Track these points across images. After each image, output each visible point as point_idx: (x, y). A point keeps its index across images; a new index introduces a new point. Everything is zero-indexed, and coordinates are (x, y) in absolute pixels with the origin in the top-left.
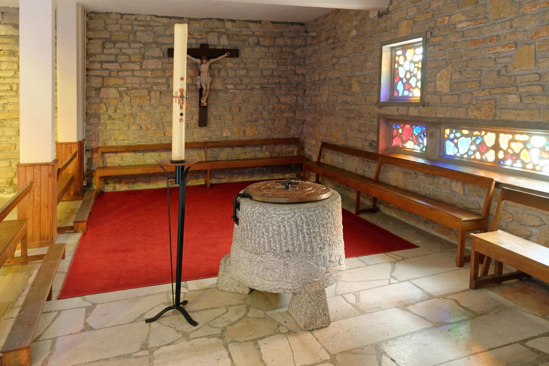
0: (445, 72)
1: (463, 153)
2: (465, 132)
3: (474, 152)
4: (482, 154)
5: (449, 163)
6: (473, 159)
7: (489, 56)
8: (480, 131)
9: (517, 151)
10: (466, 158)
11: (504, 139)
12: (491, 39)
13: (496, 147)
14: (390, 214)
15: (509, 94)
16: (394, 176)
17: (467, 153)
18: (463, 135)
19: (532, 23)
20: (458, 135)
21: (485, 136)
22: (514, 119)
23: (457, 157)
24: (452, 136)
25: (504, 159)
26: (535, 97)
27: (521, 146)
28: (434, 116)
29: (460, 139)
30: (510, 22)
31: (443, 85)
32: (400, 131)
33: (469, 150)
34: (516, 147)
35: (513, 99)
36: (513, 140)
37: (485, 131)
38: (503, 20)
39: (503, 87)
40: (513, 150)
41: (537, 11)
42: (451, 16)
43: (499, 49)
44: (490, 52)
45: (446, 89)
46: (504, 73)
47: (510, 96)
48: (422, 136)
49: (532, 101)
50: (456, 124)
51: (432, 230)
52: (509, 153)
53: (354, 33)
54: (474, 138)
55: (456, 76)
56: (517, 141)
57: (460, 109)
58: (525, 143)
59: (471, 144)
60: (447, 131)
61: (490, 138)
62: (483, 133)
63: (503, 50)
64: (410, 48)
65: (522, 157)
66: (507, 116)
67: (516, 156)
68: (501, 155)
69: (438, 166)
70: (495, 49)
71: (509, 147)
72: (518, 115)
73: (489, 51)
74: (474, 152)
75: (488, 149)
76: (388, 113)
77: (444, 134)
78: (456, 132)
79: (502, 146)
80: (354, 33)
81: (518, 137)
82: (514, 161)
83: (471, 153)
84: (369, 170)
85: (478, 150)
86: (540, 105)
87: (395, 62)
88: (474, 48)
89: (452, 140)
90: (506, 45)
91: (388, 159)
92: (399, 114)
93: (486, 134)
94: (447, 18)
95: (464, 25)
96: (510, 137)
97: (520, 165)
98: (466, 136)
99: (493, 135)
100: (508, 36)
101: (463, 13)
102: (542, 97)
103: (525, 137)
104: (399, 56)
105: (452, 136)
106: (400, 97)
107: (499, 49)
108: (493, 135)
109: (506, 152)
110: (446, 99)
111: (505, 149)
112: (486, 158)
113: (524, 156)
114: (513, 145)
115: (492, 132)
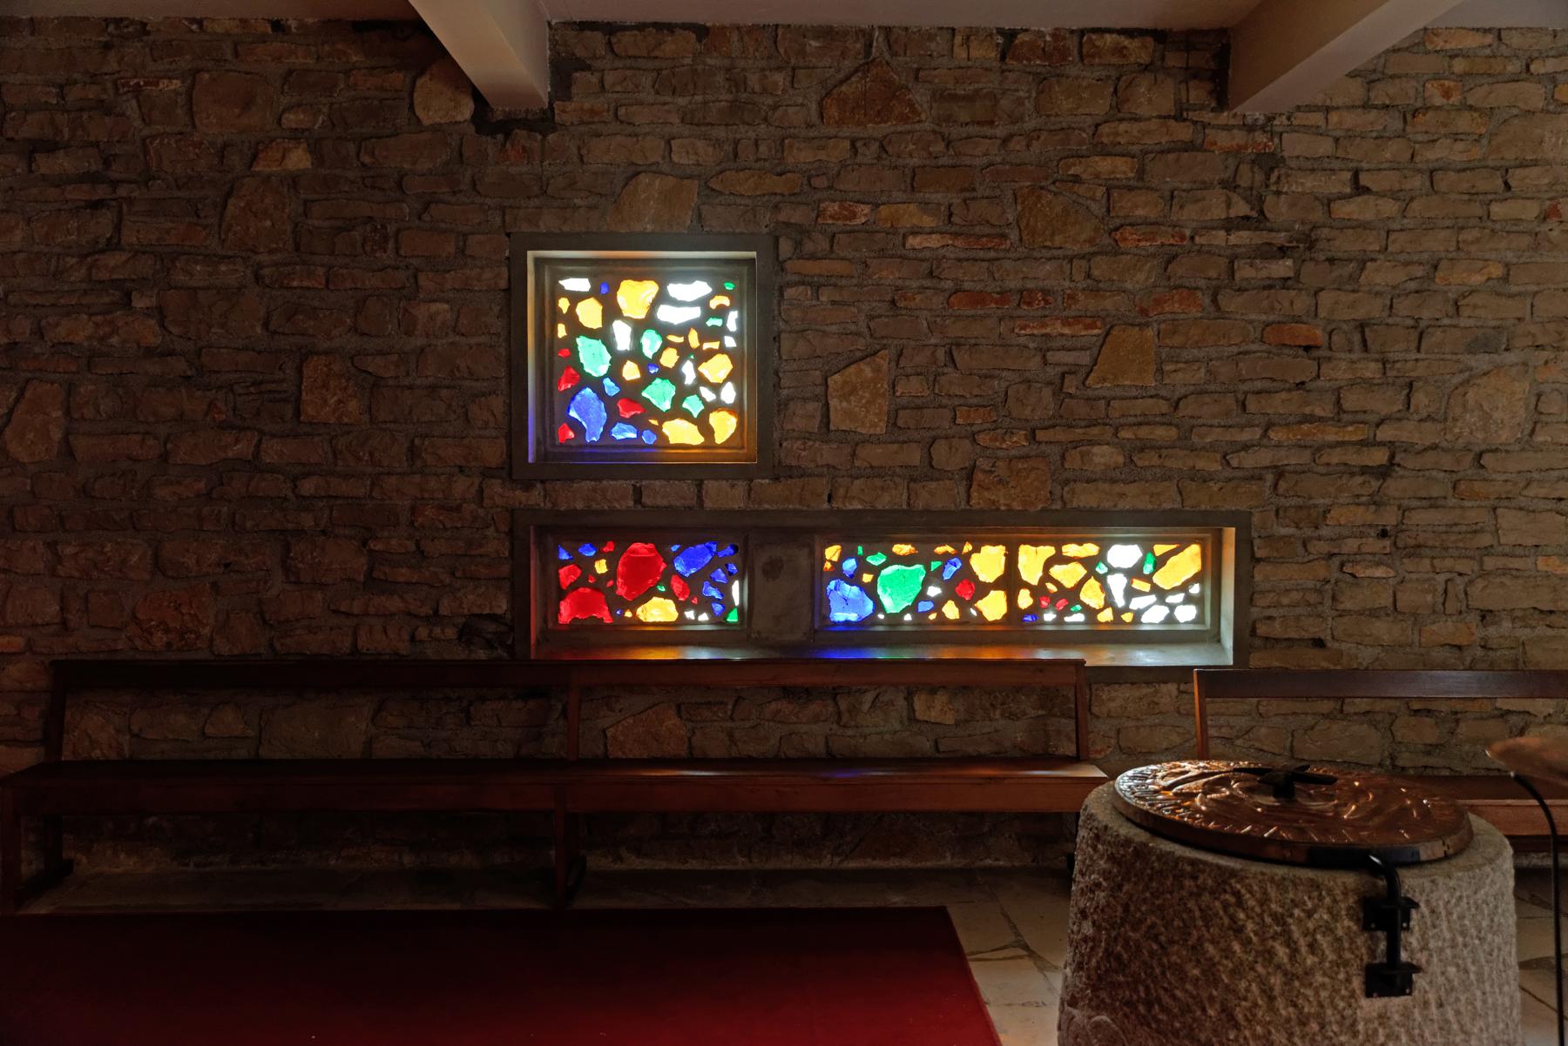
0: (868, 372)
1: (897, 610)
2: (902, 549)
3: (939, 603)
4: (963, 605)
5: (860, 646)
6: (934, 623)
7: (1022, 340)
8: (958, 543)
9: (1069, 583)
10: (909, 623)
11: (1031, 561)
12: (1025, 296)
13: (1010, 581)
14: (618, 866)
15: (1091, 443)
16: (621, 728)
17: (912, 609)
18: (894, 559)
19: (1141, 277)
20: (876, 560)
21: (974, 556)
22: (1107, 505)
23: (880, 623)
24: (849, 565)
25: (1035, 610)
26: (1164, 452)
27: (1078, 571)
28: (826, 506)
29: (884, 572)
30: (1084, 263)
31: (859, 409)
32: (601, 567)
33: (922, 596)
34: (1068, 575)
35: (1104, 456)
36: (1059, 559)
37: (971, 542)
38: (1055, 252)
39: (1070, 426)
40: (1056, 583)
41: (1152, 250)
42: (878, 205)
43: (1057, 328)
44: (1028, 331)
45: (875, 425)
46: (1072, 391)
47: (1096, 449)
48: (720, 575)
49: (1156, 461)
50: (871, 530)
51: (837, 860)
52: (1047, 593)
53: (298, 159)
54: (935, 565)
55: (913, 388)
56: (1068, 560)
57: (933, 485)
58: (1089, 563)
59: (926, 584)
60: (832, 553)
61: (988, 562)
62: (968, 548)
63: (1066, 331)
64: (639, 277)
65: (1084, 596)
66: (1086, 498)
67: (1071, 596)
68: (1025, 600)
69: (802, 659)
70: (1044, 326)
71: (1046, 577)
72: (1122, 495)
73: (1024, 328)
74: (939, 603)
75: (983, 589)
76: (579, 505)
77: (823, 560)
78: (868, 552)
79: (1025, 576)
80: (298, 159)
81: (1070, 550)
82: (1067, 611)
83: (924, 606)
84: (495, 728)
85: (951, 592)
86: (1171, 469)
87: (556, 316)
88: (972, 312)
89: (854, 579)
90: (1078, 319)
91: (604, 669)
92: (659, 509)
93: (977, 550)
94: (866, 209)
95: (934, 241)
96: (1049, 551)
97: (1080, 617)
98: (907, 560)
99: (1000, 551)
100: (1081, 297)
101: (925, 206)
102: (1181, 453)
103: (1090, 549)
104: (576, 298)
105: (849, 565)
106: (593, 445)
107: (1057, 328)
108: (1000, 551)
109: (1038, 591)
110: (873, 454)
111: (1034, 581)
112: (980, 613)
113: (1092, 595)
114: (1057, 571)
115: (995, 543)
